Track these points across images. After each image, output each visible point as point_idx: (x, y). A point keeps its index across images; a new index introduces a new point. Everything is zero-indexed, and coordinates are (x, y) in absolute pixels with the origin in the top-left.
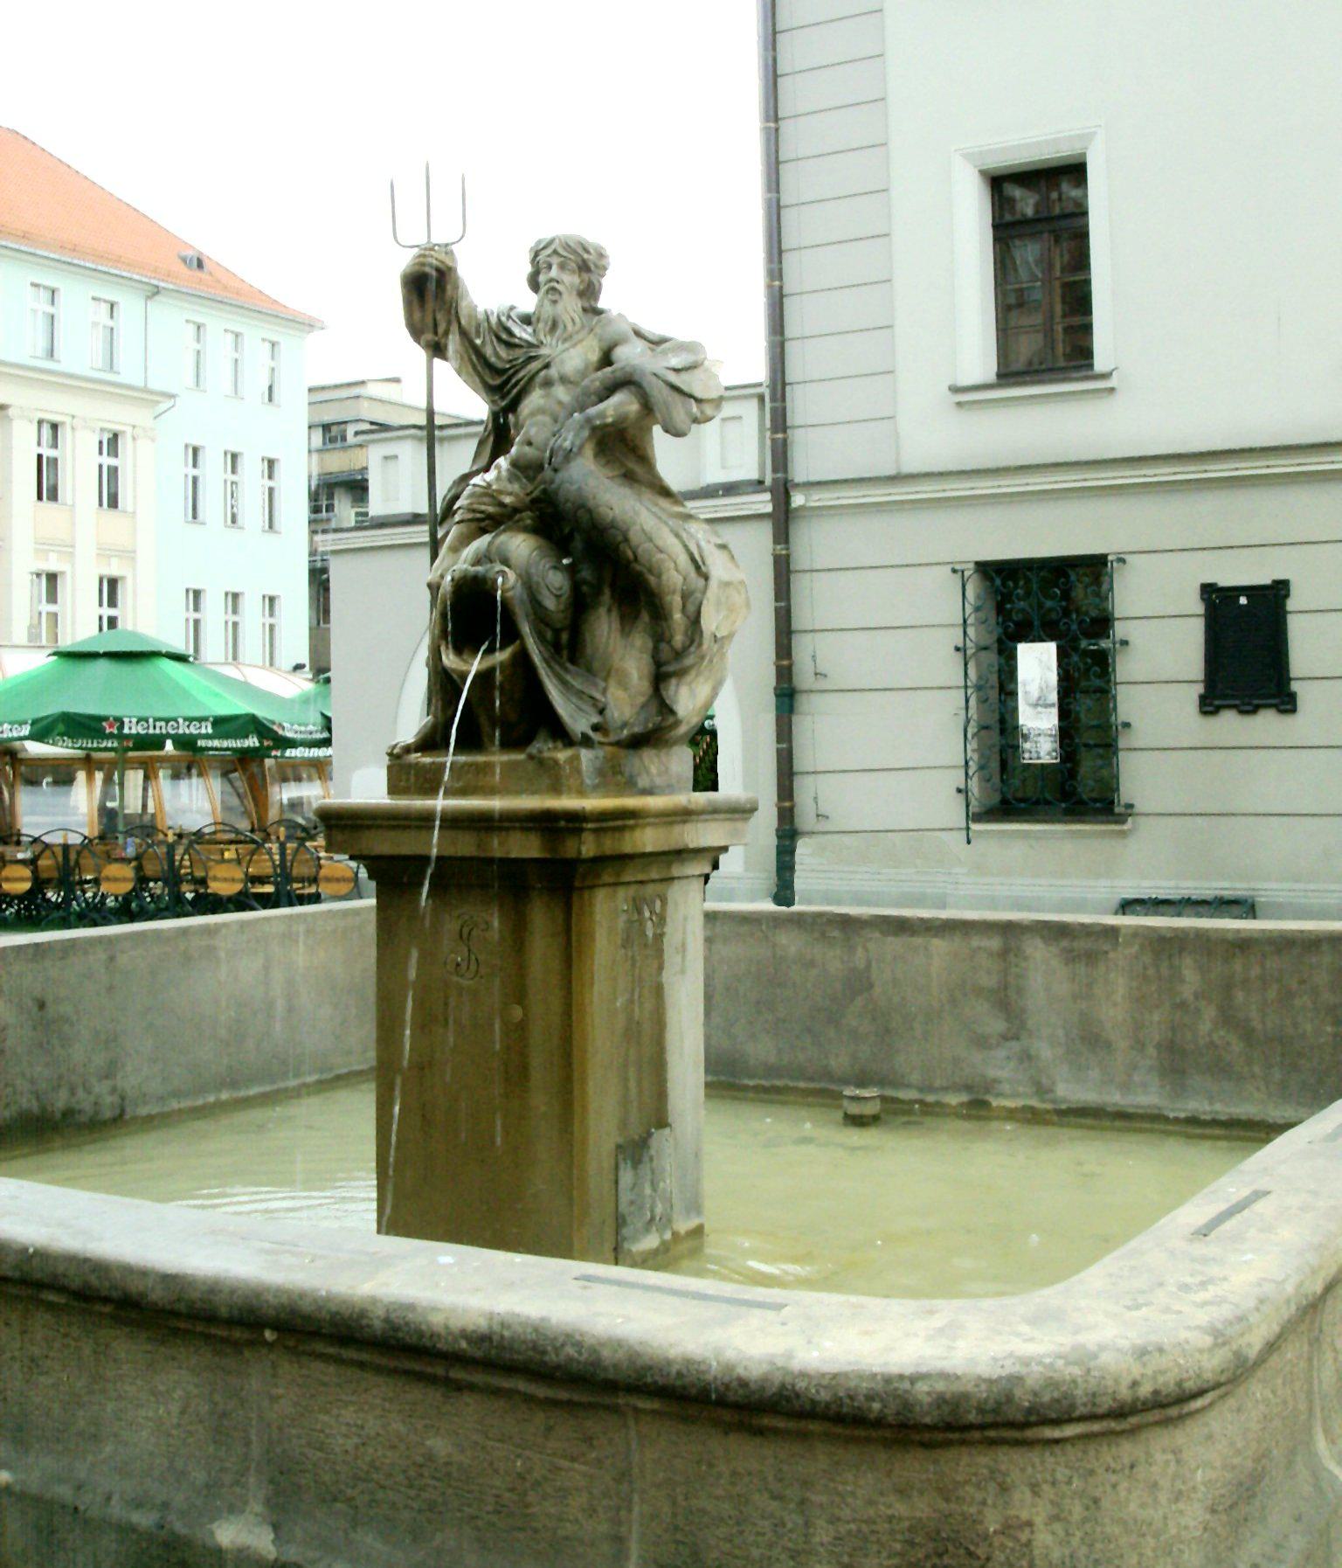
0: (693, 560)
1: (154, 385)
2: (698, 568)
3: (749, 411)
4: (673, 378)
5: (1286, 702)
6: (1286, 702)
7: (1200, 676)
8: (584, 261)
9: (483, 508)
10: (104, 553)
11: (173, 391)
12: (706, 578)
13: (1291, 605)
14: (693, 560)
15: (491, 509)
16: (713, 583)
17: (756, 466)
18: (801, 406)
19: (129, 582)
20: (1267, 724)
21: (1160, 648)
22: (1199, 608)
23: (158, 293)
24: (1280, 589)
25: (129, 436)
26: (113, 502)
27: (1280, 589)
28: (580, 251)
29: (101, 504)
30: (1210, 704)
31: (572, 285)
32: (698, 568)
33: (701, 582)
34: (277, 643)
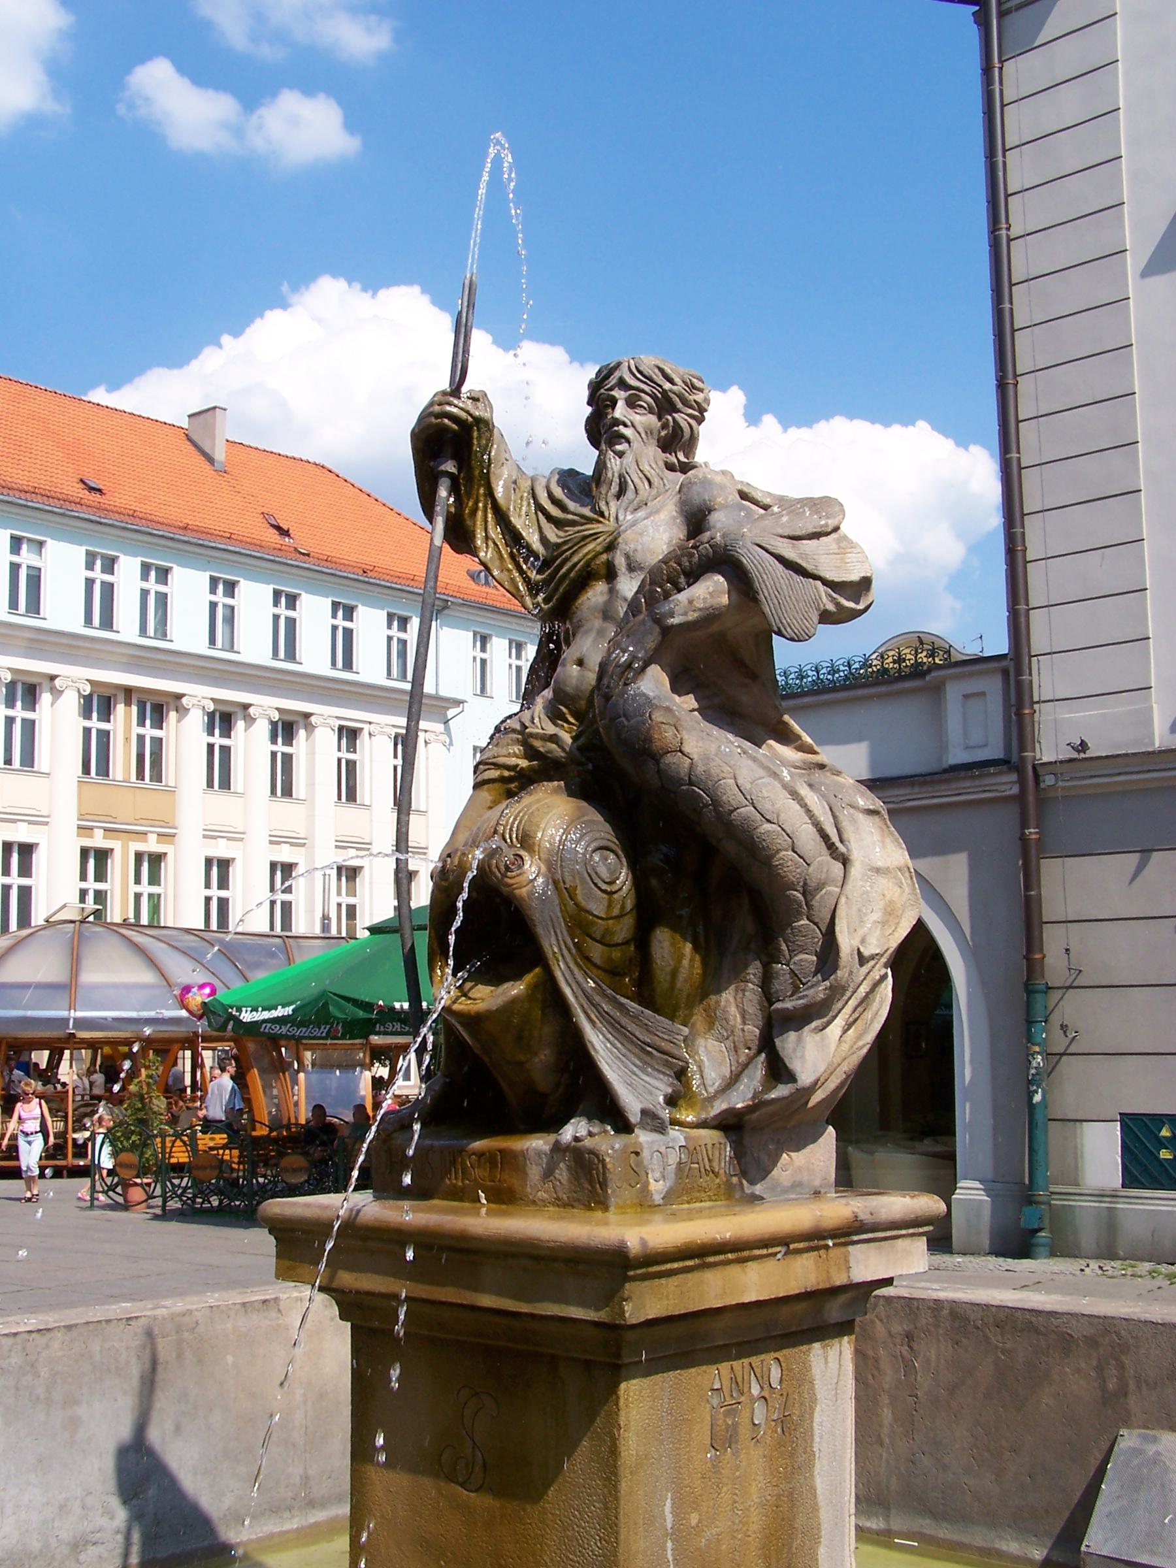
0: (825, 837)
1: (443, 693)
2: (830, 846)
3: (993, 686)
4: (789, 551)
8: (664, 393)
9: (513, 761)
10: (210, 835)
11: (460, 697)
12: (845, 861)
14: (825, 837)
15: (524, 763)
16: (855, 871)
17: (1001, 744)
18: (1046, 679)
19: (170, 858)
23: (446, 607)
25: (365, 733)
26: (352, 796)
28: (660, 379)
29: (339, 798)
31: (649, 432)
32: (830, 846)
33: (837, 867)
34: (160, 965)
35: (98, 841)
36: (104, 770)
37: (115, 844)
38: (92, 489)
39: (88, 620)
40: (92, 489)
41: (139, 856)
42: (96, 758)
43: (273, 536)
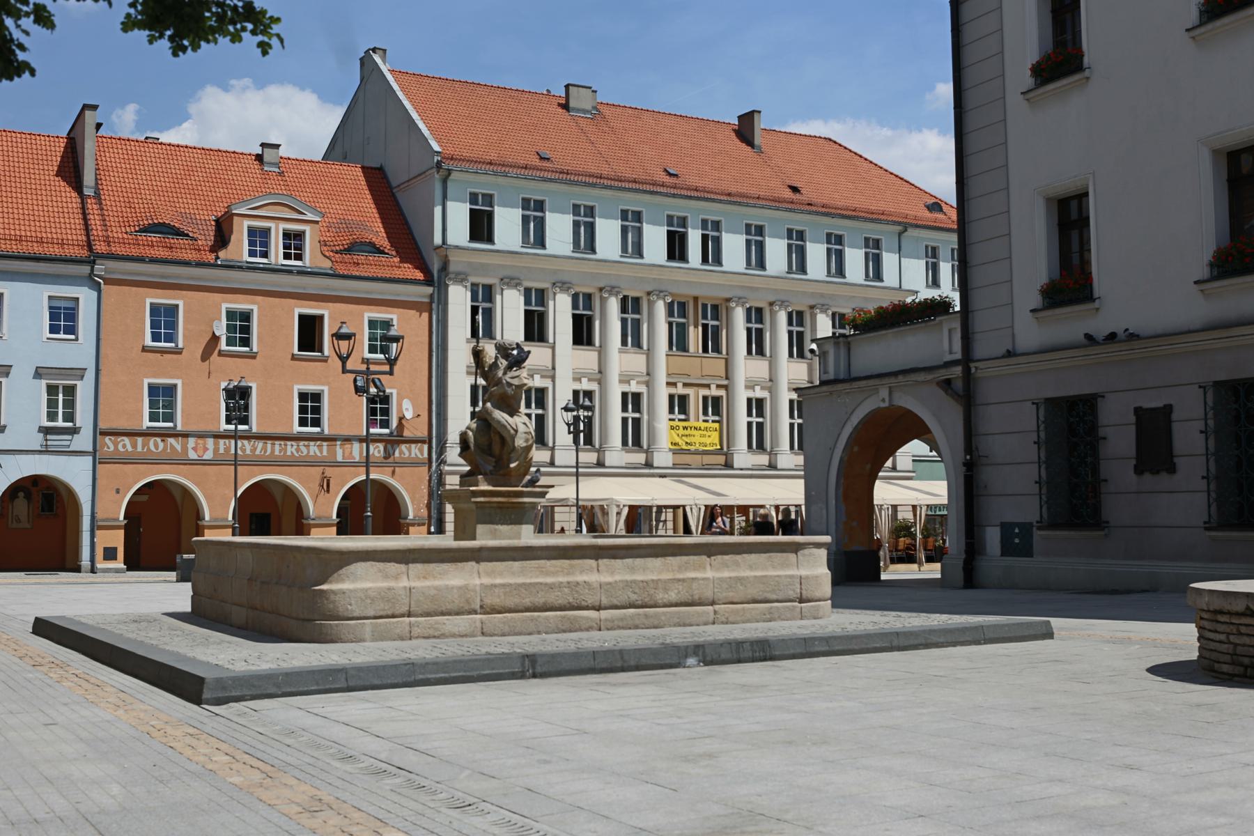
5: (1172, 469)
6: (1172, 469)
13: (1175, 416)
18: (981, 322)
20: (1164, 480)
21: (1119, 440)
22: (1133, 419)
24: (1168, 409)
27: (1168, 409)
30: (1139, 470)
35: (680, 390)
36: (683, 347)
37: (690, 391)
38: (670, 175)
40: (670, 175)
41: (705, 398)
42: (678, 341)
43: (788, 194)
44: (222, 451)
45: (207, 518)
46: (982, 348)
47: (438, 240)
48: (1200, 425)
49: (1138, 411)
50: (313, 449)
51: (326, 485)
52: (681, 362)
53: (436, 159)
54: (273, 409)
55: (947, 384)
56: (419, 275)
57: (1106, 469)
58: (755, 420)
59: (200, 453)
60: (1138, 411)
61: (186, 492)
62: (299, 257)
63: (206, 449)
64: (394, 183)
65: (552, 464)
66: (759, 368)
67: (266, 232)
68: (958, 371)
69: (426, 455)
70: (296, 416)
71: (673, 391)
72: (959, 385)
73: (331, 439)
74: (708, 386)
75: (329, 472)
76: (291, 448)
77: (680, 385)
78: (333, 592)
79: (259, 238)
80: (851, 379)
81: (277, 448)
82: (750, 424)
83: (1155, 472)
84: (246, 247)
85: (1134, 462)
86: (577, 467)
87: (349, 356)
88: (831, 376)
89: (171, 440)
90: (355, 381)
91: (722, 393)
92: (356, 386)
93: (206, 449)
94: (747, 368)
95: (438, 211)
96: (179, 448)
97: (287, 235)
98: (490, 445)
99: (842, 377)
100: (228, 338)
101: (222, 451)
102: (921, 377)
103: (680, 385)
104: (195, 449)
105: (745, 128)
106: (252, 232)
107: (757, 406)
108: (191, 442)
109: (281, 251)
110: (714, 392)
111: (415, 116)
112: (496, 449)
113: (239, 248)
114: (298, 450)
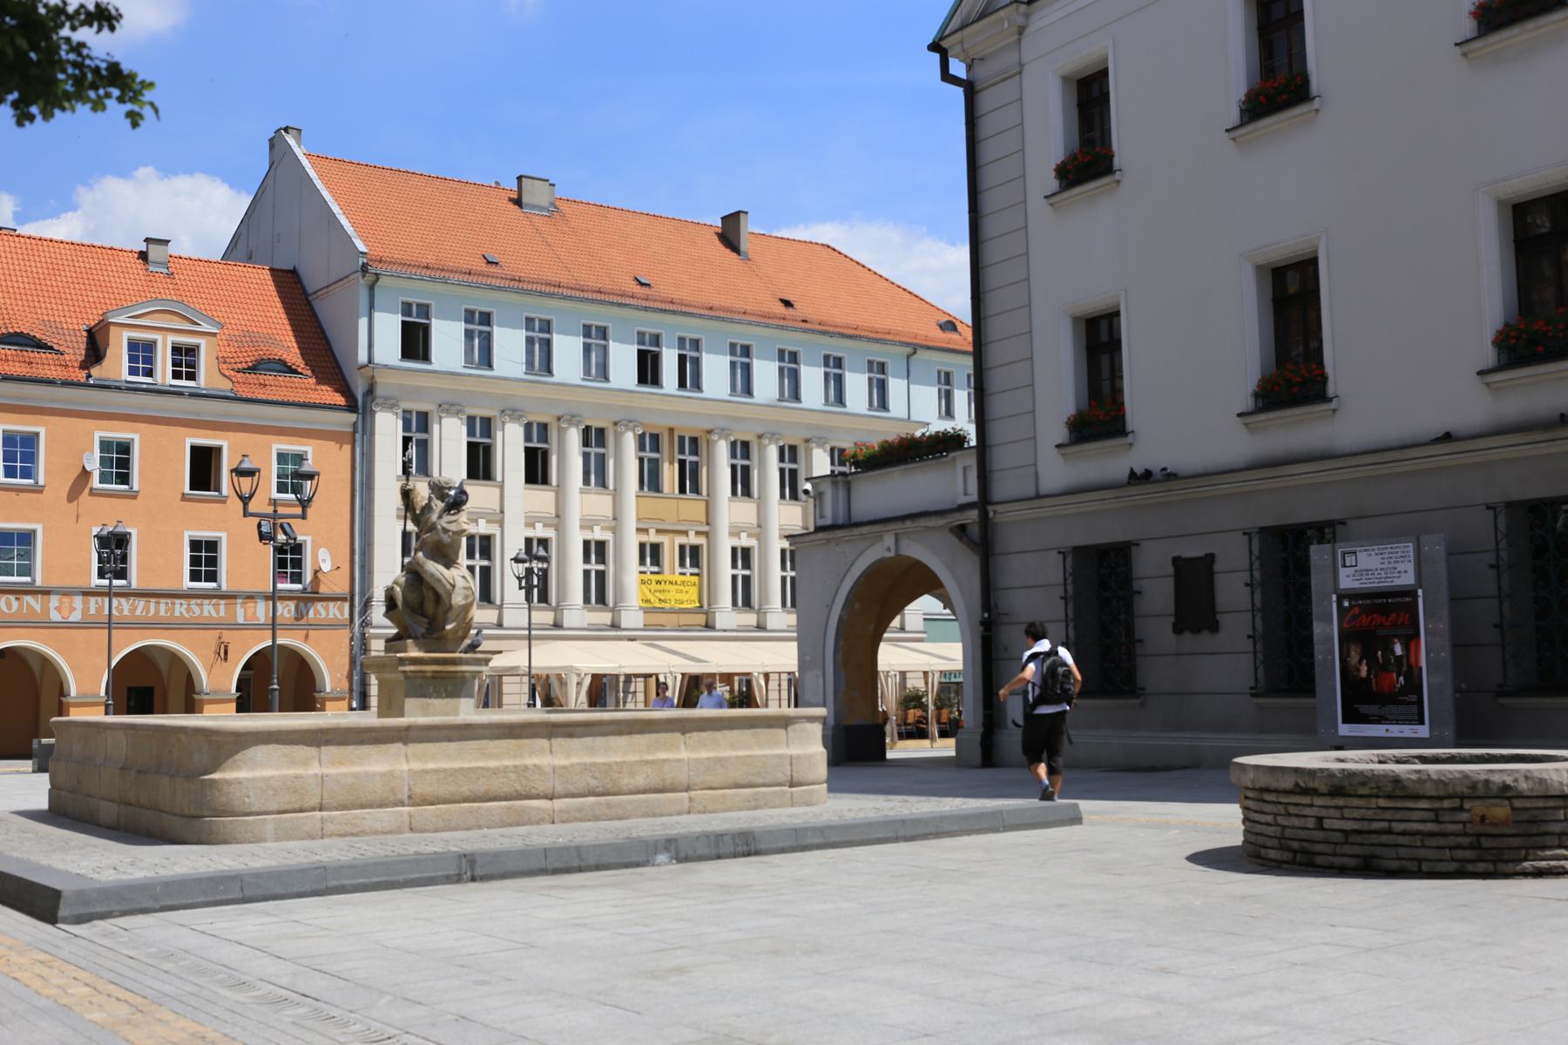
5: (1214, 627)
6: (1214, 627)
7: (1171, 609)
13: (1217, 567)
18: (1001, 458)
20: (1205, 640)
21: (1156, 593)
22: (1170, 570)
24: (1210, 559)
27: (1210, 559)
30: (1178, 629)
35: (653, 538)
38: (642, 284)
39: (587, 371)
40: (642, 284)
41: (682, 547)
44: (92, 611)
45: (73, 693)
46: (1004, 487)
47: (362, 357)
48: (1246, 577)
49: (1177, 561)
50: (208, 609)
51: (224, 653)
52: (654, 504)
53: (361, 261)
54: (158, 559)
55: (961, 531)
56: (340, 400)
57: (1143, 628)
58: (741, 572)
59: (66, 614)
60: (1177, 561)
61: (45, 661)
62: (191, 376)
63: (72, 609)
64: (310, 289)
65: (500, 625)
66: (745, 511)
67: (150, 347)
68: (974, 514)
69: (347, 615)
70: (187, 568)
71: (644, 538)
72: (975, 531)
73: (230, 597)
74: (686, 533)
75: (227, 636)
76: (180, 608)
77: (652, 532)
78: (227, 782)
79: (142, 353)
80: (851, 525)
81: (162, 608)
82: (734, 578)
83: (1196, 630)
84: (126, 364)
85: (1172, 619)
86: (529, 629)
87: (250, 497)
88: (828, 521)
89: (28, 599)
90: (259, 526)
91: (701, 541)
92: (260, 533)
93: (72, 609)
94: (731, 512)
95: (363, 323)
96: (38, 608)
97: (176, 350)
98: (422, 604)
99: (840, 522)
100: (102, 475)
101: (92, 611)
102: (933, 522)
103: (652, 532)
104: (58, 609)
105: (730, 233)
106: (133, 345)
107: (742, 556)
108: (54, 600)
109: (170, 368)
110: (692, 540)
111: (336, 209)
112: (430, 607)
113: (116, 364)
114: (188, 610)
